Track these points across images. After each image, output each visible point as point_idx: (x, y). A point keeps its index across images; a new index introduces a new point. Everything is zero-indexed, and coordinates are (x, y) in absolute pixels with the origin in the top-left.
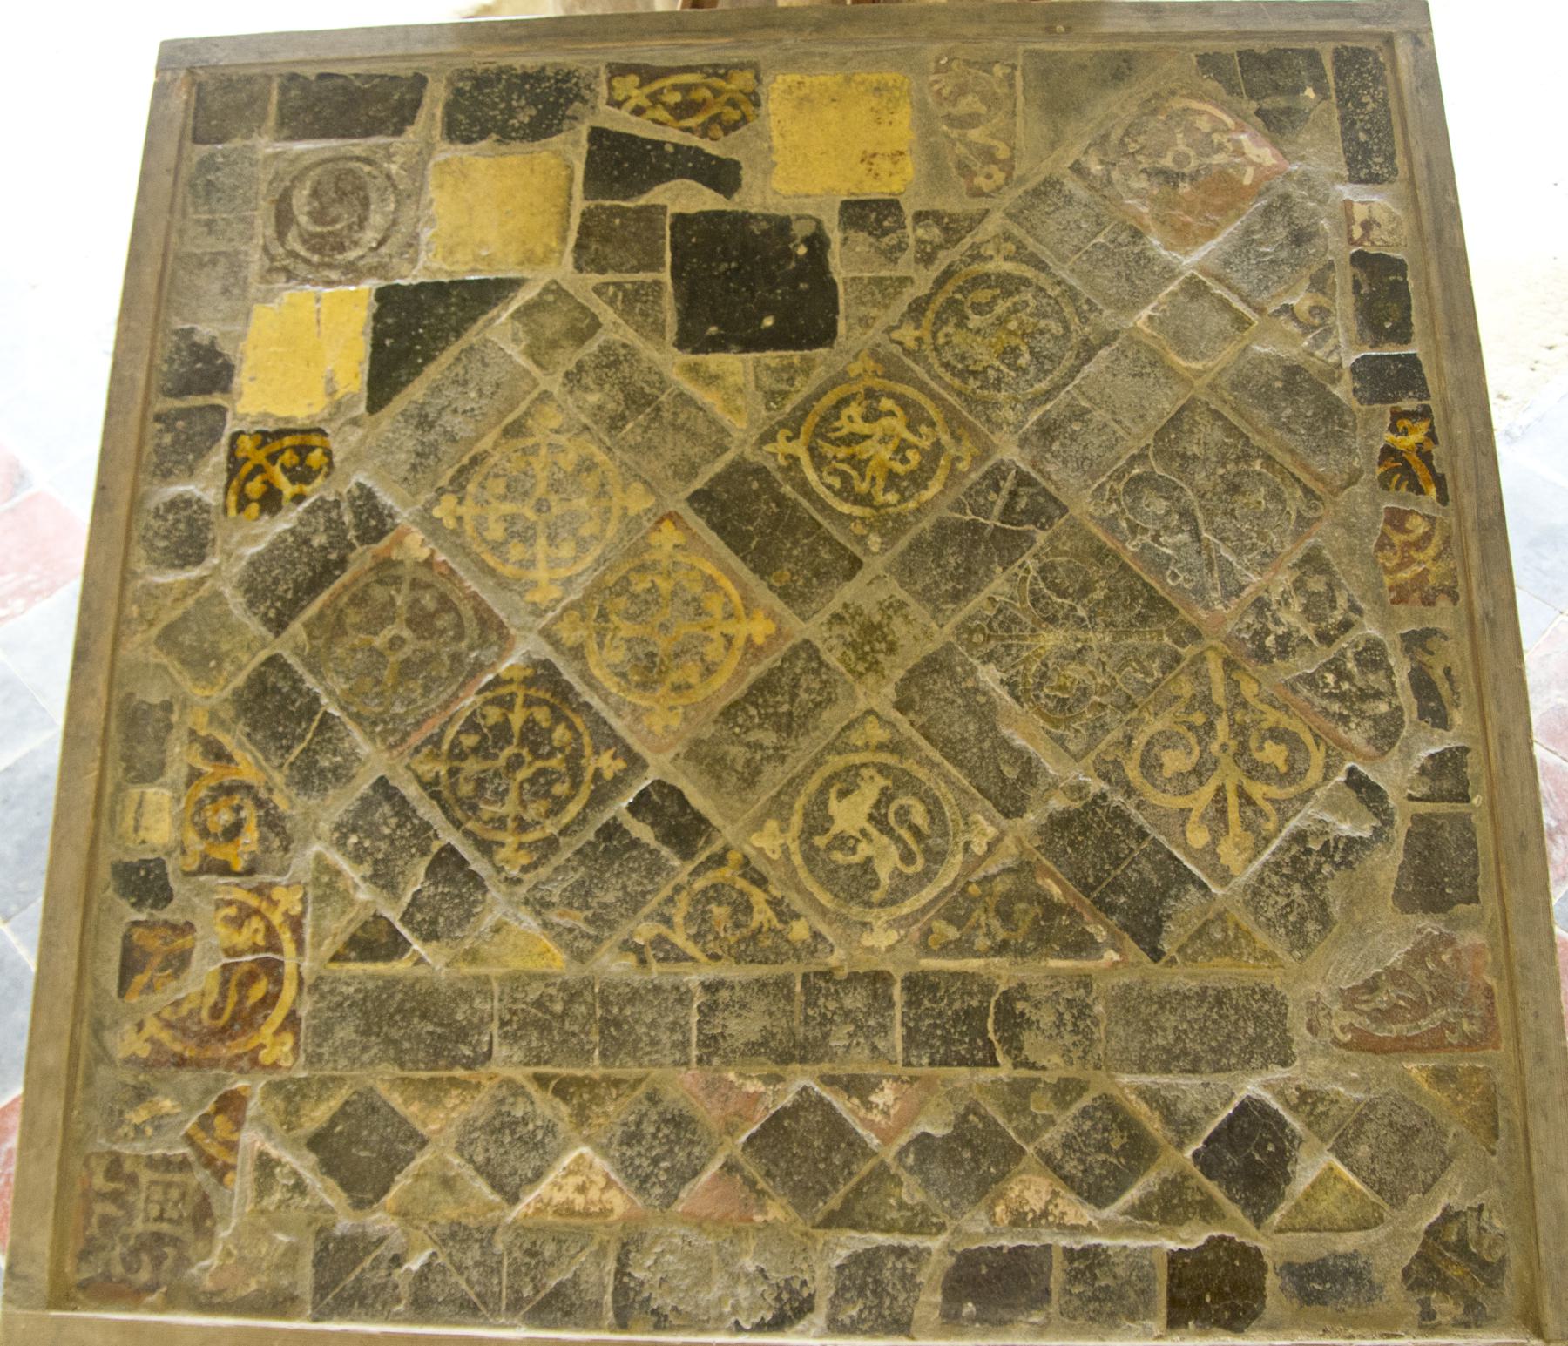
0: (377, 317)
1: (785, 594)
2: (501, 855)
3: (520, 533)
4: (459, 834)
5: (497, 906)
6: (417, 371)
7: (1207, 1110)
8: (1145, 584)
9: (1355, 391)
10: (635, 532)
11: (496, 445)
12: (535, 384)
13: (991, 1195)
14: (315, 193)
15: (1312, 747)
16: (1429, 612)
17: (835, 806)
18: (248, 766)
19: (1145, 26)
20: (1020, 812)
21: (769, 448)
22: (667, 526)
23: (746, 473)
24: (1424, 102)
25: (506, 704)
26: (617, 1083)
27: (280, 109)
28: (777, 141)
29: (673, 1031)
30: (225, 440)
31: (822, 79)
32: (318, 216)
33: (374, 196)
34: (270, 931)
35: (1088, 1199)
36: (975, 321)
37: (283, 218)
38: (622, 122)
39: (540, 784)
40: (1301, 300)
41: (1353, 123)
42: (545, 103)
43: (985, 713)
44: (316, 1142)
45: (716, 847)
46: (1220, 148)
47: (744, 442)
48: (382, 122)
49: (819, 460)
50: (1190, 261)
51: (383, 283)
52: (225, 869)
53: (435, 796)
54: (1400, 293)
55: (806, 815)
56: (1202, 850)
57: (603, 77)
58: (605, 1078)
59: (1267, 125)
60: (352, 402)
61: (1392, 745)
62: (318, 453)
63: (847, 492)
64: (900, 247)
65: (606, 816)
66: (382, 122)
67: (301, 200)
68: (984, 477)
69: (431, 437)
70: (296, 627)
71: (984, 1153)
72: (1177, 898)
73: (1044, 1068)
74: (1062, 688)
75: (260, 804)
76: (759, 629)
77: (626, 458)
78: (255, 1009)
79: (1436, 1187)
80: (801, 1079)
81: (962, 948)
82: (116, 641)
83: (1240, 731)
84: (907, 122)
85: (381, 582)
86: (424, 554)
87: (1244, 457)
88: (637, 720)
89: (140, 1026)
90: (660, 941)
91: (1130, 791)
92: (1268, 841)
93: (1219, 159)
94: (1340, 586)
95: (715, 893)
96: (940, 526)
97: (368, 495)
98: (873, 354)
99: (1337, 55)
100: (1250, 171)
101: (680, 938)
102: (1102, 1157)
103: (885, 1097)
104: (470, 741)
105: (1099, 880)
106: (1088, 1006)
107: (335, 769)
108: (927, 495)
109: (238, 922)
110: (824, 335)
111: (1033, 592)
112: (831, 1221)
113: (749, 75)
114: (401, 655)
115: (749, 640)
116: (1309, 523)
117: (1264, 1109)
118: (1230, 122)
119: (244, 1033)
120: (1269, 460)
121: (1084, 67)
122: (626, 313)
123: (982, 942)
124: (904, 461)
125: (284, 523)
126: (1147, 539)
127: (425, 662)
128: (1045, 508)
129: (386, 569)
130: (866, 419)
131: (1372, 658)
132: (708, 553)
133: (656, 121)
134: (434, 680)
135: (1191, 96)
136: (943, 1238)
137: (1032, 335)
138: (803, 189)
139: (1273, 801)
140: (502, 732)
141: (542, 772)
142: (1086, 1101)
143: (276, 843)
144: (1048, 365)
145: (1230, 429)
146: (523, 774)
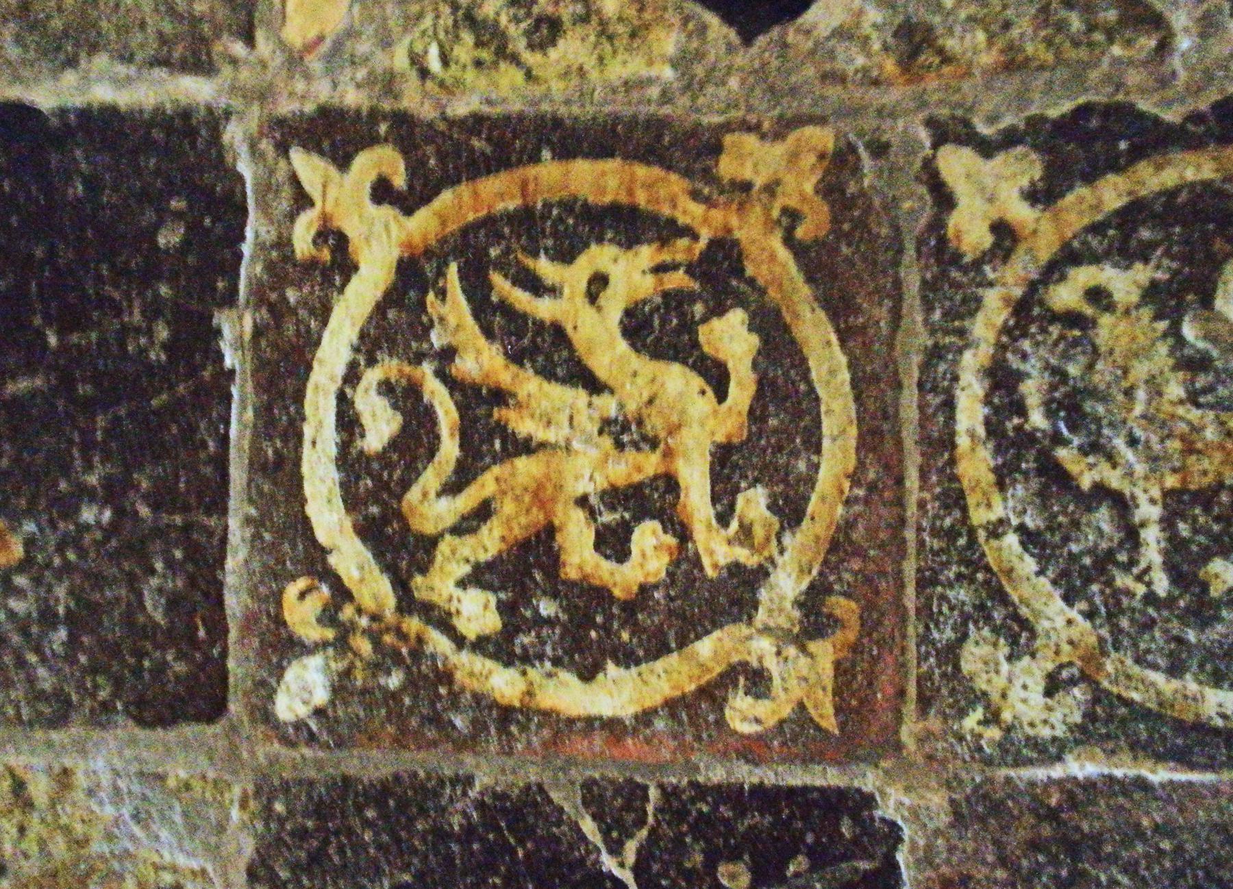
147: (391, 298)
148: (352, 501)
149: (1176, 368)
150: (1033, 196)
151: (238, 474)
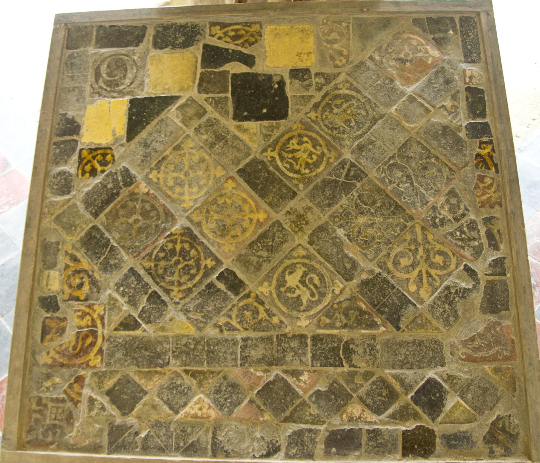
0: (130, 109)
1: (270, 204)
2: (173, 294)
3: (179, 183)
4: (158, 287)
5: (171, 312)
6: (144, 128)
7: (416, 382)
8: (394, 201)
9: (467, 134)
10: (219, 183)
11: (171, 153)
12: (184, 132)
13: (341, 411)
14: (108, 66)
15: (452, 257)
16: (492, 211)
17: (287, 277)
19: (394, 9)
20: (351, 279)
21: (265, 154)
22: (230, 181)
23: (257, 163)
24: (491, 35)
25: (174, 242)
26: (212, 373)
27: (96, 37)
28: (267, 49)
29: (232, 354)
30: (77, 151)
31: (283, 27)
32: (110, 74)
33: (129, 68)
34: (93, 320)
35: (375, 412)
36: (336, 110)
37: (98, 75)
38: (214, 42)
40: (448, 103)
42: (188, 36)
43: (339, 245)
44: (109, 393)
45: (247, 291)
46: (420, 51)
47: (256, 152)
48: (132, 42)
49: (282, 158)
50: (410, 90)
51: (132, 97)
52: (77, 299)
53: (150, 274)
54: (482, 101)
55: (277, 280)
56: (414, 292)
57: (208, 26)
59: (436, 43)
60: (121, 138)
61: (479, 256)
62: (109, 156)
63: (292, 169)
64: (310, 85)
65: (209, 281)
66: (132, 42)
67: (104, 69)
69: (149, 150)
71: (339, 397)
72: (405, 309)
73: (359, 367)
74: (366, 237)
75: (89, 276)
76: (262, 216)
77: (216, 157)
78: (88, 347)
79: (495, 408)
80: (276, 371)
81: (331, 326)
83: (427, 251)
84: (312, 42)
85: (131, 200)
86: (146, 190)
87: (429, 157)
88: (219, 248)
89: (48, 353)
90: (227, 324)
91: (389, 272)
92: (437, 289)
93: (420, 55)
94: (462, 202)
95: (246, 307)
96: (324, 181)
97: (127, 170)
98: (301, 122)
99: (461, 19)
100: (431, 59)
101: (234, 323)
102: (379, 398)
103: (305, 377)
104: (162, 255)
105: (378, 303)
106: (375, 346)
107: (115, 265)
108: (319, 170)
109: (82, 317)
110: (284, 115)
111: (356, 204)
112: (286, 420)
113: (258, 26)
114: (138, 225)
115: (258, 220)
116: (451, 180)
117: (435, 382)
118: (424, 42)
119: (84, 355)
120: (437, 158)
121: (373, 23)
122: (216, 108)
123: (338, 324)
124: (311, 158)
125: (98, 180)
127: (146, 228)
128: (360, 175)
130: (298, 144)
131: (472, 226)
132: (244, 190)
133: (226, 42)
134: (149, 234)
135: (410, 33)
136: (325, 426)
137: (355, 115)
138: (277, 65)
139: (438, 276)
141: (187, 266)
142: (374, 379)
143: (95, 290)
144: (361, 126)
145: (424, 148)
146: (180, 266)
147: (280, 157)
148: (291, 172)
149: (316, 442)
150: (316, 113)
151: (282, 178)
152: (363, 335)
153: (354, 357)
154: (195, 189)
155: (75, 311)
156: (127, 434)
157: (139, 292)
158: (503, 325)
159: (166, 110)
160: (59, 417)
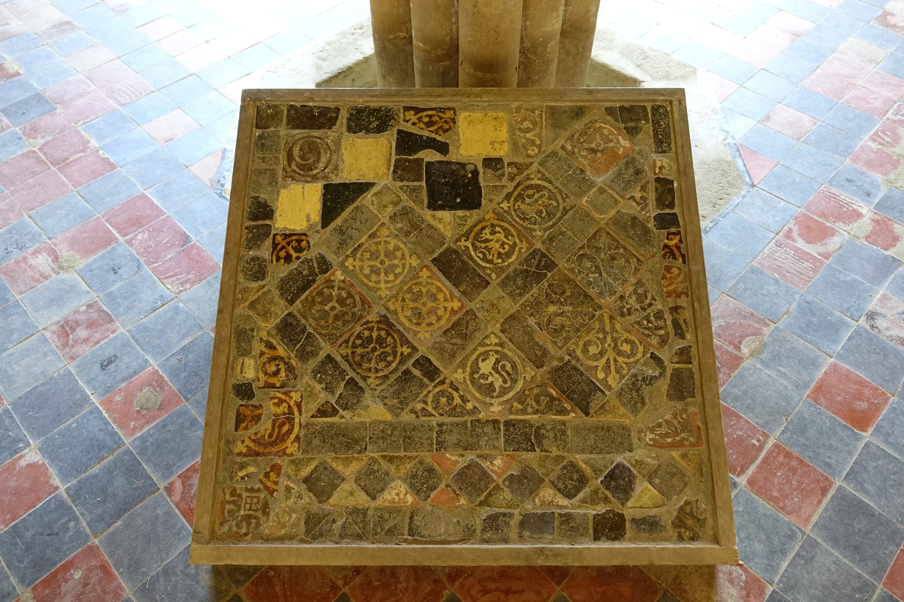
0: (324, 195)
1: (464, 293)
2: (369, 381)
3: (375, 271)
4: (355, 374)
5: (368, 399)
6: (339, 214)
7: (605, 466)
8: (583, 291)
9: (655, 225)
10: (414, 275)
11: (366, 241)
12: (380, 220)
13: (533, 495)
14: (301, 149)
15: (639, 346)
16: (678, 300)
17: (481, 364)
18: (281, 351)
19: (587, 97)
20: (542, 366)
21: (459, 244)
22: (425, 270)
23: (451, 252)
24: (682, 125)
25: (371, 329)
26: (409, 458)
27: (288, 118)
28: (461, 137)
29: (427, 440)
30: (271, 236)
31: (477, 114)
32: (303, 158)
33: (322, 151)
34: (290, 407)
35: (566, 496)
36: (528, 200)
37: (290, 158)
38: (409, 128)
39: (383, 357)
40: (638, 195)
41: (657, 132)
42: (382, 120)
43: (530, 334)
44: (306, 481)
45: (441, 378)
46: (611, 141)
47: (450, 242)
48: (324, 124)
49: (475, 248)
50: (599, 180)
51: (327, 183)
52: (273, 386)
53: (347, 361)
54: (671, 191)
55: (471, 367)
56: (602, 379)
57: (402, 111)
58: (405, 456)
59: (628, 133)
60: (316, 224)
61: (666, 345)
62: (305, 242)
63: (485, 259)
64: (503, 175)
65: (405, 367)
66: (324, 124)
67: (296, 151)
68: (530, 254)
69: (344, 237)
70: (298, 302)
71: (531, 481)
72: (594, 395)
73: (551, 452)
74: (555, 325)
75: (285, 363)
76: (456, 305)
77: (411, 246)
78: (284, 434)
79: (682, 493)
80: (471, 456)
81: (524, 412)
82: (233, 308)
83: (615, 340)
84: (505, 131)
85: (327, 287)
86: (343, 278)
87: (617, 248)
88: (415, 335)
89: (243, 442)
90: (423, 409)
91: (578, 360)
92: (624, 377)
93: (611, 144)
94: (649, 292)
95: (442, 393)
96: (515, 270)
97: (323, 257)
98: (494, 212)
99: (653, 108)
100: (621, 149)
101: (430, 409)
102: (570, 482)
103: (498, 462)
104: (359, 342)
105: (568, 389)
106: (565, 431)
107: (312, 352)
108: (511, 260)
109: (278, 405)
110: (478, 205)
111: (546, 293)
112: (481, 504)
113: (452, 112)
114: (335, 312)
115: (452, 308)
116: (639, 270)
117: (624, 466)
118: (616, 132)
119: (281, 443)
120: (625, 248)
121: (566, 112)
122: (410, 196)
123: (530, 410)
124: (504, 248)
125: (295, 265)
126: (584, 275)
127: (343, 315)
128: (551, 265)
129: (329, 283)
130: (491, 234)
131: (659, 315)
132: (440, 281)
133: (420, 128)
134: (346, 321)
135: (602, 122)
136: (518, 510)
137: (546, 206)
138: (470, 154)
139: (626, 363)
140: (369, 340)
141: (383, 353)
142: (565, 463)
143: (292, 377)
144: (552, 216)
145: (613, 239)
146: (377, 353)
152: (554, 421)
153: (545, 442)
154: (391, 277)
155: (272, 398)
156: (323, 522)
157: (336, 379)
158: (689, 411)
159: (361, 198)
160: (254, 507)
